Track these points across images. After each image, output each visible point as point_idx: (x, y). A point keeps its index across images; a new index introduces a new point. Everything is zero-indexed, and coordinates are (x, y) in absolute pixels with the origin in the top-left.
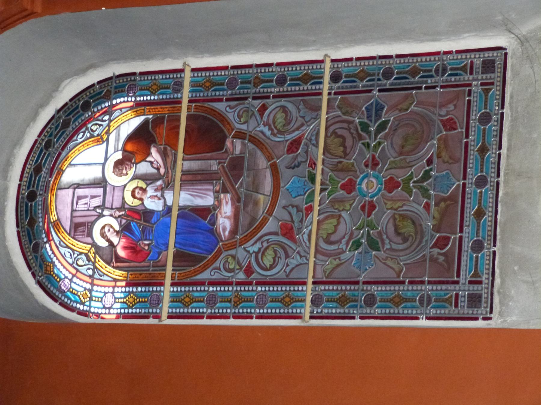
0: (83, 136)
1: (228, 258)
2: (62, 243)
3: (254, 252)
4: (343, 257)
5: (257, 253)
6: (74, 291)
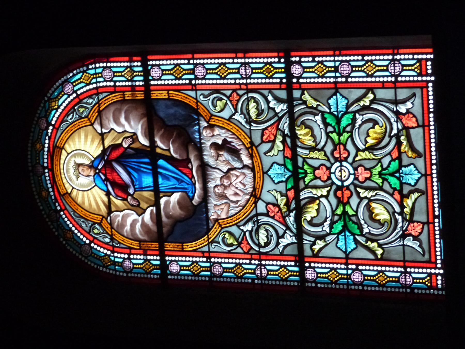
0: (73, 116)
1: (225, 234)
2: (76, 214)
3: (247, 230)
4: (328, 238)
5: (251, 232)
6: (96, 256)
